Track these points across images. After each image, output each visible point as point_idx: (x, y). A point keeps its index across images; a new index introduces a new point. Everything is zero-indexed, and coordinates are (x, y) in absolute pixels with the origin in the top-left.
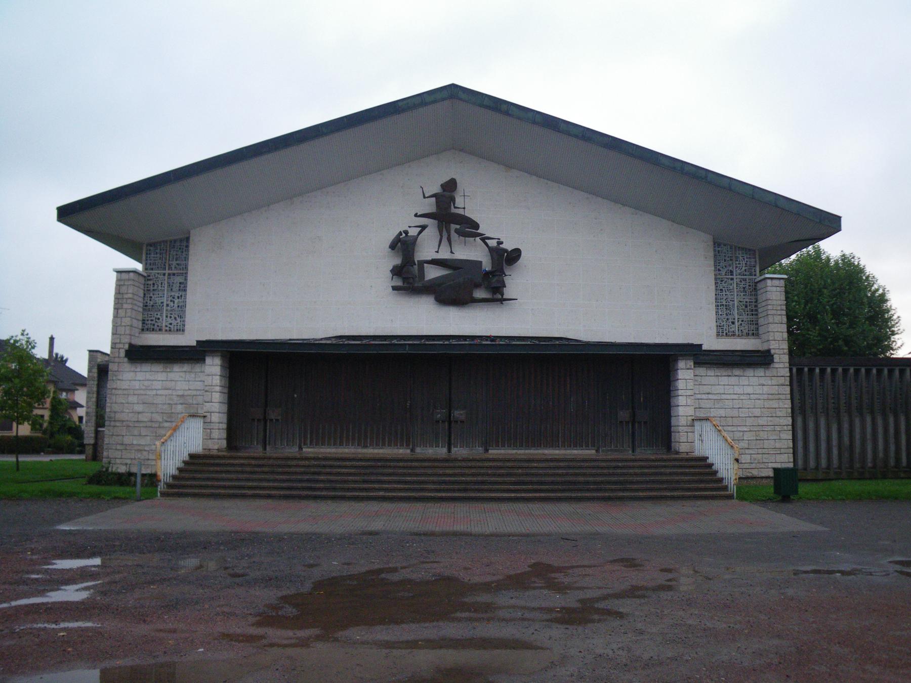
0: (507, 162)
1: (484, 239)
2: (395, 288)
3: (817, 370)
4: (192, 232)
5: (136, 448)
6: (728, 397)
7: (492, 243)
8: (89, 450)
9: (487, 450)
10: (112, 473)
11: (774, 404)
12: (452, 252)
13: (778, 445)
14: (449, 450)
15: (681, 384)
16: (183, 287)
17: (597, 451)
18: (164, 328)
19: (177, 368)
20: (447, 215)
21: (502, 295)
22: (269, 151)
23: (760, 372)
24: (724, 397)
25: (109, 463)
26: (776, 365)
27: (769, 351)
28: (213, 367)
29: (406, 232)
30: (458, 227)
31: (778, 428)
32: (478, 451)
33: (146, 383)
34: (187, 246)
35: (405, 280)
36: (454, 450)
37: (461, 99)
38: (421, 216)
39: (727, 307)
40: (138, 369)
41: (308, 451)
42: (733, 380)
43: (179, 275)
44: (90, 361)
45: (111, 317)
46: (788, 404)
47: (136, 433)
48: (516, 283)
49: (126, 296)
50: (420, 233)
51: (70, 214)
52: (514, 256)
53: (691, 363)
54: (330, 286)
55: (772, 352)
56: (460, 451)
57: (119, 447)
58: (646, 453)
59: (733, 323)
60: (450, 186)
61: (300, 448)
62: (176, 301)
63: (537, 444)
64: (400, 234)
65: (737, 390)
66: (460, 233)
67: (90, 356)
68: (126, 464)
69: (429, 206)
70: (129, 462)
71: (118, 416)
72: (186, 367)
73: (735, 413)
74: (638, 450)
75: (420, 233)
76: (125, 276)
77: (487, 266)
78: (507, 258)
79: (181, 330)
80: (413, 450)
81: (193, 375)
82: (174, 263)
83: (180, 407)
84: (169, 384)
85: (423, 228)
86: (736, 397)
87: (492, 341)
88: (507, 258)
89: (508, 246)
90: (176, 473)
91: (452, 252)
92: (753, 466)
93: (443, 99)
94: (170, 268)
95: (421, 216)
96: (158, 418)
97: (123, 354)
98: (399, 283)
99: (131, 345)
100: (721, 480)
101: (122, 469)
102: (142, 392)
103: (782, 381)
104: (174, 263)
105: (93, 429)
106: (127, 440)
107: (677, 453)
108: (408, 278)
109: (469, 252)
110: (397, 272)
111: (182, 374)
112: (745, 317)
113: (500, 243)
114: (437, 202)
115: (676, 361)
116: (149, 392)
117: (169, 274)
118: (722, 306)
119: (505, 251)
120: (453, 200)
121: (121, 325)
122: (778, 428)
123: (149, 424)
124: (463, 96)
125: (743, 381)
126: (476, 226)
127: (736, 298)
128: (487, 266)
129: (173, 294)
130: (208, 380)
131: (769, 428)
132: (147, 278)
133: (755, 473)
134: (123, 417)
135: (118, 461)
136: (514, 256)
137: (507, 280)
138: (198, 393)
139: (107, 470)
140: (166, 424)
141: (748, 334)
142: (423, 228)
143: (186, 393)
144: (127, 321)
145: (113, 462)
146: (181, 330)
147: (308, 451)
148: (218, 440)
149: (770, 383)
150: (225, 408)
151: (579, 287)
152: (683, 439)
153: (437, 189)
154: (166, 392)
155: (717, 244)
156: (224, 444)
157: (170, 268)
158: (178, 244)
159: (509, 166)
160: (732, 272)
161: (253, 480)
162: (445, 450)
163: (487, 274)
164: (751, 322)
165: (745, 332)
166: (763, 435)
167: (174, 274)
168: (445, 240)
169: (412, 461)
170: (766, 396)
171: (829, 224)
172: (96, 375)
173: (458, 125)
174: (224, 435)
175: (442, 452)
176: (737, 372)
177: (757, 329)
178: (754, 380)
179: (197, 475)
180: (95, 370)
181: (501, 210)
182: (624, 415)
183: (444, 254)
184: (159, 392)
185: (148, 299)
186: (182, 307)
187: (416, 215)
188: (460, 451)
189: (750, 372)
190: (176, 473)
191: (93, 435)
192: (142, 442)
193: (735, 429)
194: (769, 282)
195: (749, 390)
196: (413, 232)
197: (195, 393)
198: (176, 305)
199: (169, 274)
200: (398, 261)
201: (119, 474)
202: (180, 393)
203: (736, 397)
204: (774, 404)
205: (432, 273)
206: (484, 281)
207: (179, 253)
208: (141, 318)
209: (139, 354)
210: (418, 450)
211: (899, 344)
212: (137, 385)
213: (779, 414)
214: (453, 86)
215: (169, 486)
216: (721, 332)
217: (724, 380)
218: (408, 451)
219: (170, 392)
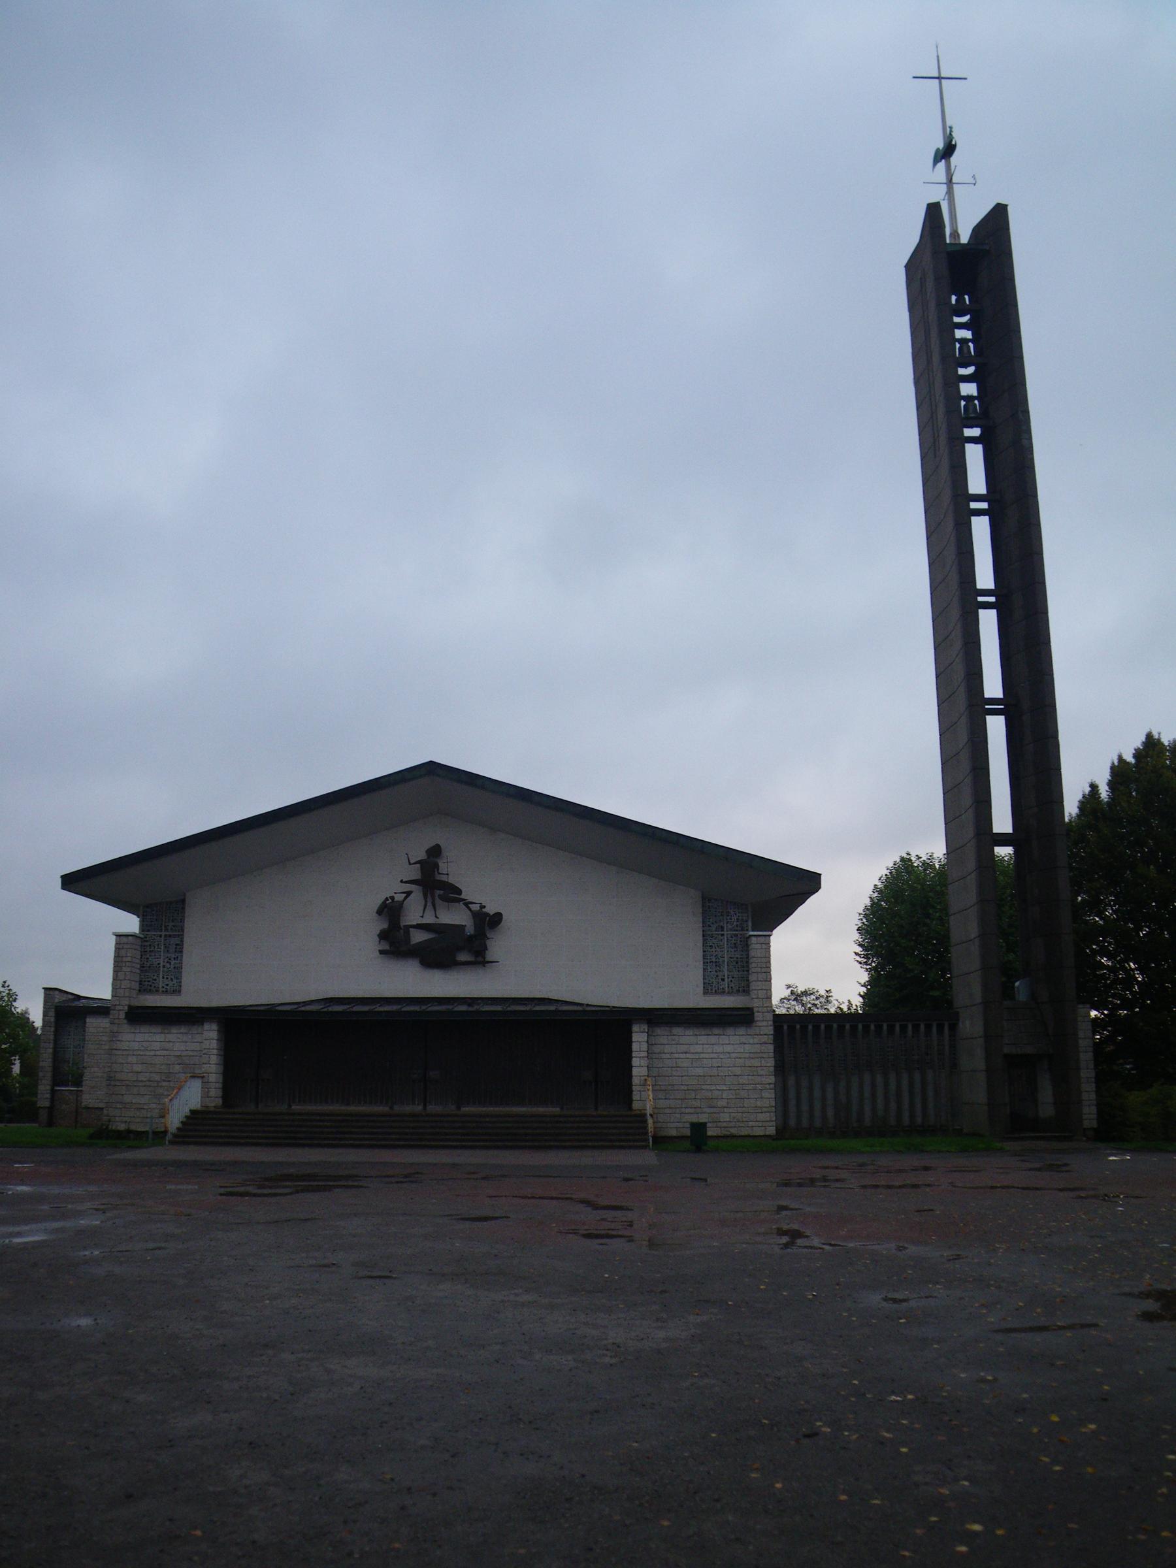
1: (467, 904)
2: (381, 952)
6: (707, 1056)
7: (475, 908)
8: (43, 1116)
9: (459, 1108)
11: (756, 1063)
13: (759, 1104)
16: (179, 949)
17: (562, 1108)
20: (432, 881)
23: (742, 1031)
24: (702, 1056)
28: (210, 1034)
29: (392, 898)
31: (759, 1087)
34: (183, 908)
38: (406, 882)
39: (717, 964)
42: (713, 1039)
43: (175, 936)
44: (46, 1002)
45: (111, 980)
46: (771, 1063)
48: (498, 946)
50: (406, 898)
51: (74, 882)
53: (645, 1027)
54: (319, 952)
56: (432, 1108)
57: (118, 1106)
59: (723, 980)
60: (435, 852)
61: (290, 1106)
62: (173, 962)
64: (387, 899)
66: (443, 898)
67: (46, 994)
69: (415, 873)
70: (128, 1120)
71: (118, 1076)
72: (183, 1029)
73: (714, 1072)
75: (406, 898)
76: (124, 940)
77: (470, 930)
78: (489, 922)
79: (177, 991)
80: (391, 1108)
82: (171, 924)
83: (177, 1067)
85: (408, 894)
86: (715, 1056)
87: (469, 1005)
88: (489, 922)
89: (491, 909)
90: (180, 1125)
92: (732, 1124)
93: (421, 776)
95: (406, 882)
96: (157, 1078)
97: (122, 1015)
98: (385, 946)
99: (130, 1007)
103: (765, 1039)
104: (171, 924)
105: (49, 1088)
106: (127, 1099)
108: (395, 941)
110: (383, 936)
113: (483, 907)
115: (874, 991)
118: (710, 962)
119: (487, 914)
120: (437, 866)
122: (759, 1087)
125: (724, 1040)
126: (459, 892)
128: (470, 930)
130: (206, 1044)
131: (751, 1087)
132: (143, 940)
133: (734, 1131)
137: (488, 943)
140: (164, 1084)
142: (408, 894)
144: (126, 984)
146: (177, 991)
148: (216, 1092)
150: (221, 1069)
151: (562, 951)
153: (422, 856)
155: (703, 898)
156: (220, 1102)
157: (166, 930)
160: (722, 928)
162: (420, 1108)
163: (471, 937)
166: (743, 1094)
168: (429, 904)
170: (664, 1056)
171: (1094, 787)
172: (53, 1019)
173: (436, 794)
174: (220, 1093)
175: (418, 1108)
176: (716, 1031)
177: (748, 986)
179: (198, 1127)
180: (52, 1013)
181: (484, 876)
183: (429, 919)
185: (142, 960)
186: (178, 969)
188: (432, 1108)
189: (730, 1031)
190: (180, 1125)
191: (48, 1096)
193: (713, 1088)
194: (754, 939)
195: (729, 1049)
196: (399, 897)
202: (178, 1054)
203: (715, 1056)
204: (756, 1063)
205: (418, 937)
206: (470, 944)
208: (137, 979)
209: (139, 1016)
212: (136, 1046)
213: (762, 1073)
214: (431, 763)
215: (175, 1136)
216: (707, 991)
217: (703, 1039)
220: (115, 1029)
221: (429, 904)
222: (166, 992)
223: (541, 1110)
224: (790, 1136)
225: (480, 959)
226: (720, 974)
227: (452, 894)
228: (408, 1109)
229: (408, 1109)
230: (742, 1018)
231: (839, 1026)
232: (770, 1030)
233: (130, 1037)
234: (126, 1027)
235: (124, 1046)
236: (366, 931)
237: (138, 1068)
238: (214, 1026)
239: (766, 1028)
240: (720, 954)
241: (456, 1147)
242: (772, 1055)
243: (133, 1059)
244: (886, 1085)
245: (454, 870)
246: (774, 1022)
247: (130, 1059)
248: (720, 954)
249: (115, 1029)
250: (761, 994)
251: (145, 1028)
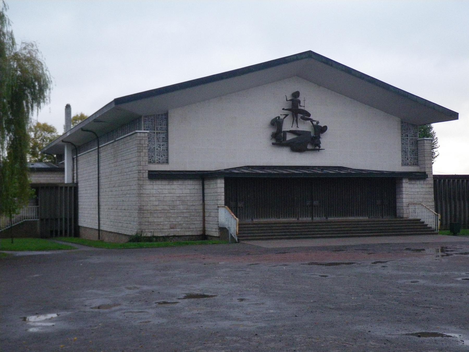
0: (320, 83)
1: (312, 121)
3: (442, 181)
4: (169, 111)
5: (156, 223)
10: (145, 237)
11: (427, 196)
12: (297, 127)
14: (312, 219)
15: (404, 189)
16: (166, 140)
17: (369, 218)
18: (156, 161)
19: (175, 183)
20: (296, 110)
21: (320, 147)
22: (227, 78)
23: (422, 182)
25: (142, 232)
26: (428, 179)
27: (425, 173)
29: (279, 117)
30: (302, 115)
32: (323, 219)
33: (159, 191)
35: (277, 140)
36: (314, 218)
37: (313, 58)
38: (286, 110)
39: (405, 152)
40: (154, 184)
41: (255, 221)
46: (433, 196)
47: (155, 215)
48: (325, 140)
49: (144, 145)
52: (323, 129)
53: (407, 181)
55: (427, 173)
56: (317, 219)
58: (386, 218)
60: (296, 95)
62: (162, 147)
63: (345, 215)
64: (276, 118)
65: (413, 190)
66: (303, 118)
68: (151, 232)
69: (288, 105)
70: (152, 231)
71: (145, 208)
72: (180, 182)
74: (384, 217)
80: (298, 219)
81: (184, 186)
83: (178, 202)
84: (172, 191)
86: (412, 193)
89: (322, 124)
91: (297, 127)
94: (157, 130)
96: (166, 207)
98: (274, 141)
100: (430, 228)
101: (149, 235)
102: (157, 195)
104: (159, 126)
106: (151, 220)
107: (403, 218)
108: (279, 139)
109: (305, 127)
111: (179, 186)
112: (412, 156)
114: (292, 103)
116: (161, 195)
117: (157, 133)
119: (321, 127)
121: (143, 161)
123: (163, 211)
124: (313, 56)
126: (309, 115)
127: (409, 148)
128: (312, 134)
129: (160, 143)
134: (148, 208)
135: (147, 230)
136: (323, 129)
138: (188, 195)
139: (141, 235)
140: (171, 211)
141: (413, 164)
142: (286, 115)
143: (181, 195)
145: (143, 231)
146: (167, 162)
147: (255, 221)
149: (425, 187)
151: (354, 145)
152: (405, 212)
154: (171, 195)
157: (157, 130)
158: (160, 117)
159: (320, 85)
160: (407, 135)
161: (372, 233)
162: (311, 219)
164: (415, 159)
165: (413, 163)
167: (159, 133)
168: (295, 121)
169: (297, 223)
170: (424, 193)
173: (310, 67)
175: (309, 219)
177: (418, 162)
178: (420, 186)
181: (321, 108)
182: (379, 202)
183: (294, 128)
184: (167, 195)
187: (283, 109)
188: (317, 219)
189: (418, 182)
192: (159, 220)
195: (418, 190)
196: (282, 117)
197: (185, 195)
198: (161, 149)
199: (157, 133)
200: (274, 130)
201: (148, 237)
202: (178, 195)
203: (412, 193)
205: (289, 137)
206: (309, 141)
207: (161, 122)
210: (300, 219)
211: (436, 154)
212: (154, 192)
213: (429, 201)
214: (310, 52)
216: (404, 164)
218: (296, 219)
219: (173, 195)
220: (141, 183)
221: (295, 121)
222: (159, 163)
223: (361, 218)
224: (245, 232)
225: (318, 148)
226: (407, 156)
227: (306, 115)
228: (304, 219)
229: (304, 219)
230: (421, 176)
231: (448, 180)
232: (432, 182)
233: (150, 187)
234: (148, 182)
235: (148, 192)
236: (265, 134)
237: (157, 203)
238: (223, 181)
239: (430, 181)
240: (407, 147)
241: (365, 236)
242: (433, 193)
243: (154, 199)
244: (460, 204)
245: (307, 104)
246: (433, 178)
247: (151, 199)
248: (407, 147)
249: (141, 183)
250: (429, 166)
251: (159, 182)
